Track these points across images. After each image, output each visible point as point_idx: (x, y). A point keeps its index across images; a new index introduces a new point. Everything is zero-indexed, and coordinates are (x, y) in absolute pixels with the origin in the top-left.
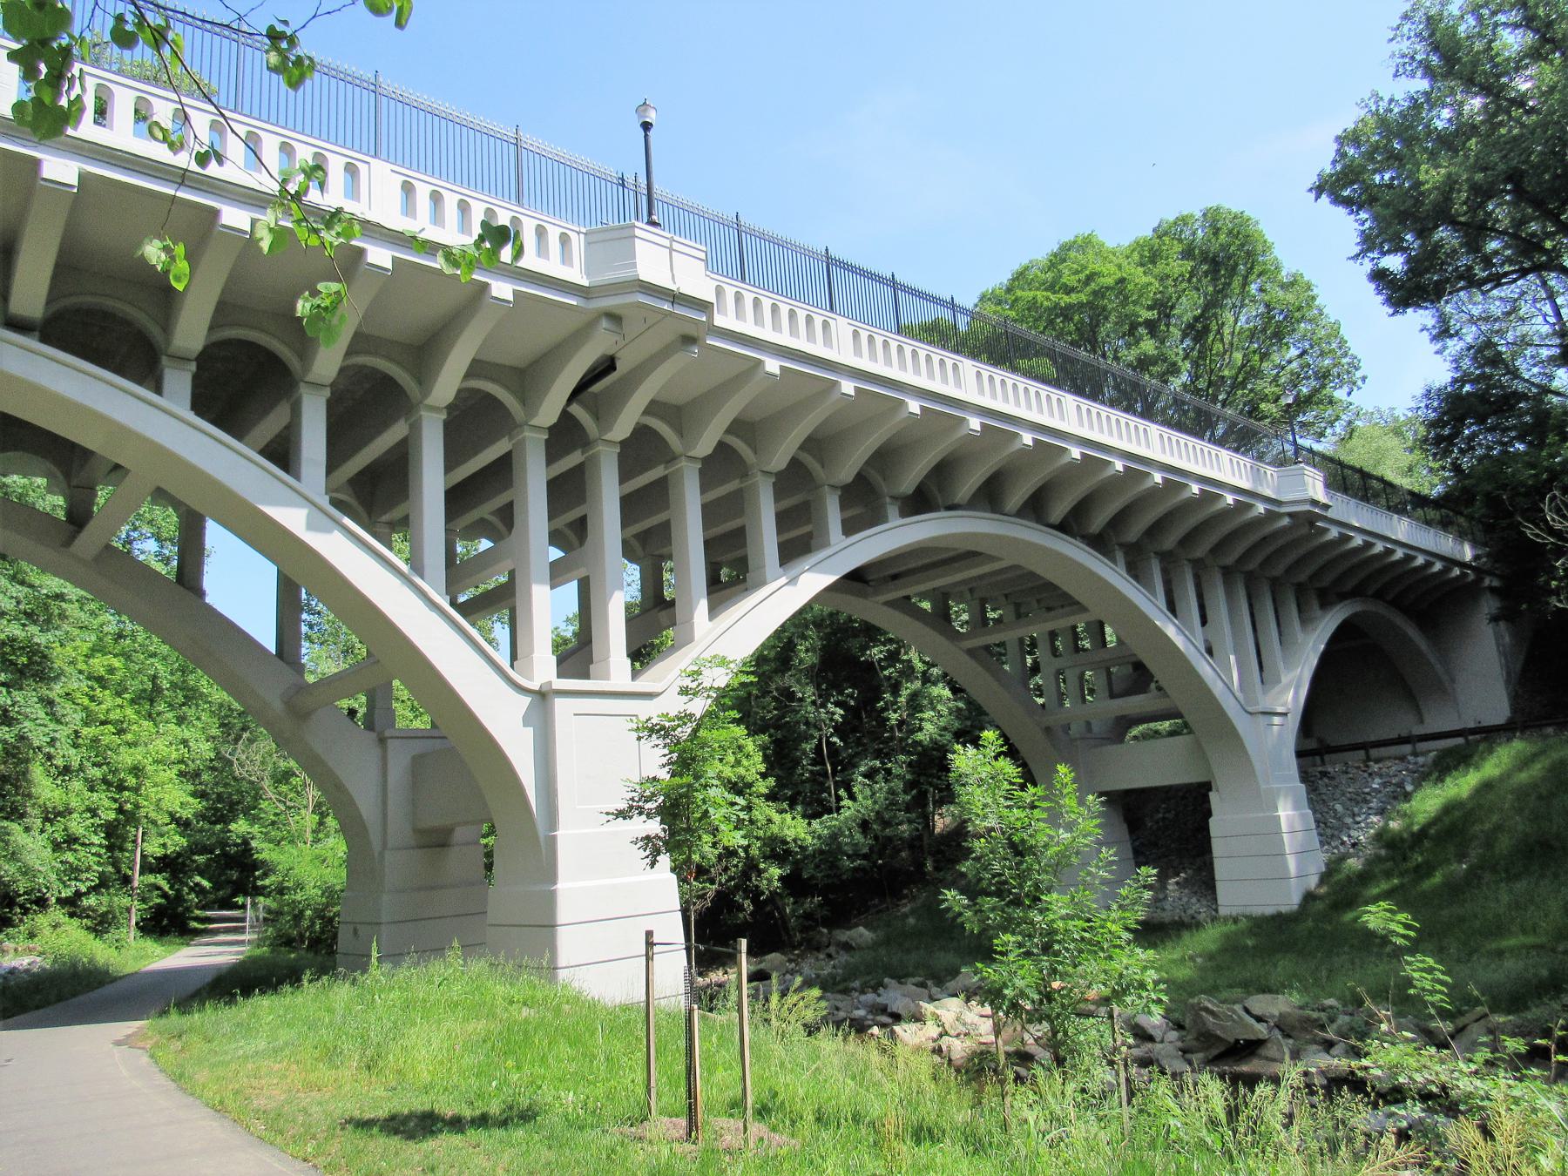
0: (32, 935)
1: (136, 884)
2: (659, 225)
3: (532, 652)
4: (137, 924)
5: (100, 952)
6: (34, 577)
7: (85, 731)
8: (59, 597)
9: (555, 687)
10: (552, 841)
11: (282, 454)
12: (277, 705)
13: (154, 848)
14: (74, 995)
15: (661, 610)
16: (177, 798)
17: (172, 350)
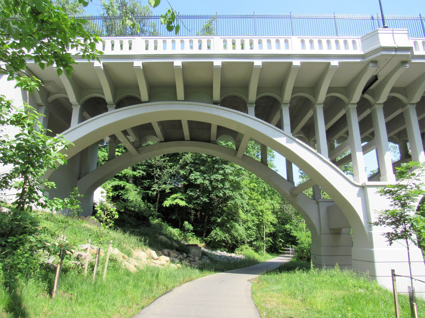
0: (242, 250)
1: (264, 240)
2: (387, 27)
3: (358, 174)
4: (266, 250)
5: (256, 256)
6: (235, 165)
7: (250, 202)
8: (241, 169)
9: (367, 184)
10: (371, 234)
11: (280, 125)
12: (288, 193)
13: (267, 231)
14: (248, 266)
15: (408, 158)
16: (271, 218)
17: (249, 102)
